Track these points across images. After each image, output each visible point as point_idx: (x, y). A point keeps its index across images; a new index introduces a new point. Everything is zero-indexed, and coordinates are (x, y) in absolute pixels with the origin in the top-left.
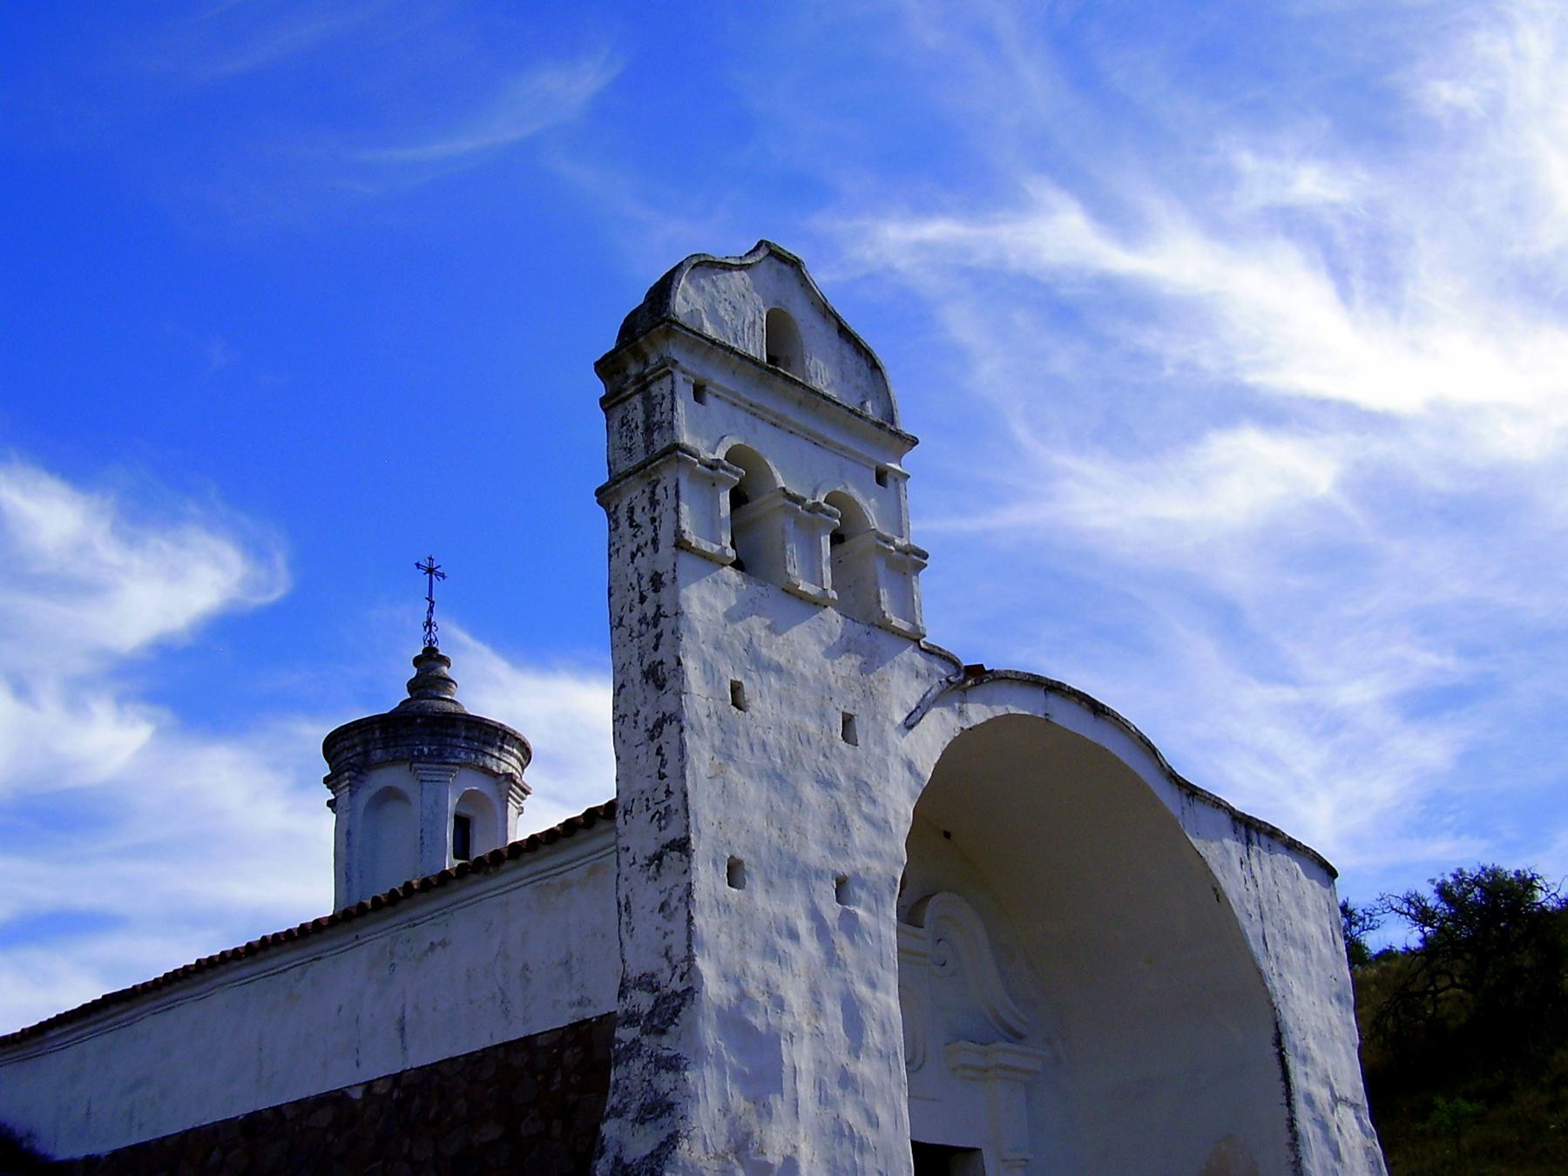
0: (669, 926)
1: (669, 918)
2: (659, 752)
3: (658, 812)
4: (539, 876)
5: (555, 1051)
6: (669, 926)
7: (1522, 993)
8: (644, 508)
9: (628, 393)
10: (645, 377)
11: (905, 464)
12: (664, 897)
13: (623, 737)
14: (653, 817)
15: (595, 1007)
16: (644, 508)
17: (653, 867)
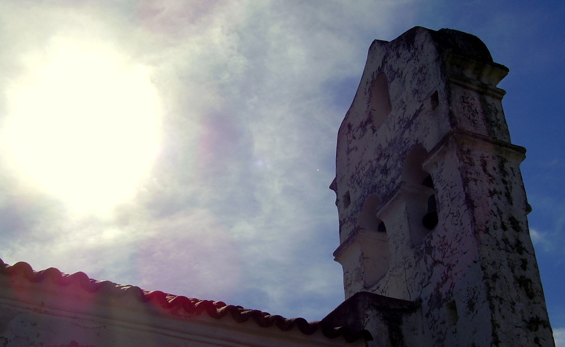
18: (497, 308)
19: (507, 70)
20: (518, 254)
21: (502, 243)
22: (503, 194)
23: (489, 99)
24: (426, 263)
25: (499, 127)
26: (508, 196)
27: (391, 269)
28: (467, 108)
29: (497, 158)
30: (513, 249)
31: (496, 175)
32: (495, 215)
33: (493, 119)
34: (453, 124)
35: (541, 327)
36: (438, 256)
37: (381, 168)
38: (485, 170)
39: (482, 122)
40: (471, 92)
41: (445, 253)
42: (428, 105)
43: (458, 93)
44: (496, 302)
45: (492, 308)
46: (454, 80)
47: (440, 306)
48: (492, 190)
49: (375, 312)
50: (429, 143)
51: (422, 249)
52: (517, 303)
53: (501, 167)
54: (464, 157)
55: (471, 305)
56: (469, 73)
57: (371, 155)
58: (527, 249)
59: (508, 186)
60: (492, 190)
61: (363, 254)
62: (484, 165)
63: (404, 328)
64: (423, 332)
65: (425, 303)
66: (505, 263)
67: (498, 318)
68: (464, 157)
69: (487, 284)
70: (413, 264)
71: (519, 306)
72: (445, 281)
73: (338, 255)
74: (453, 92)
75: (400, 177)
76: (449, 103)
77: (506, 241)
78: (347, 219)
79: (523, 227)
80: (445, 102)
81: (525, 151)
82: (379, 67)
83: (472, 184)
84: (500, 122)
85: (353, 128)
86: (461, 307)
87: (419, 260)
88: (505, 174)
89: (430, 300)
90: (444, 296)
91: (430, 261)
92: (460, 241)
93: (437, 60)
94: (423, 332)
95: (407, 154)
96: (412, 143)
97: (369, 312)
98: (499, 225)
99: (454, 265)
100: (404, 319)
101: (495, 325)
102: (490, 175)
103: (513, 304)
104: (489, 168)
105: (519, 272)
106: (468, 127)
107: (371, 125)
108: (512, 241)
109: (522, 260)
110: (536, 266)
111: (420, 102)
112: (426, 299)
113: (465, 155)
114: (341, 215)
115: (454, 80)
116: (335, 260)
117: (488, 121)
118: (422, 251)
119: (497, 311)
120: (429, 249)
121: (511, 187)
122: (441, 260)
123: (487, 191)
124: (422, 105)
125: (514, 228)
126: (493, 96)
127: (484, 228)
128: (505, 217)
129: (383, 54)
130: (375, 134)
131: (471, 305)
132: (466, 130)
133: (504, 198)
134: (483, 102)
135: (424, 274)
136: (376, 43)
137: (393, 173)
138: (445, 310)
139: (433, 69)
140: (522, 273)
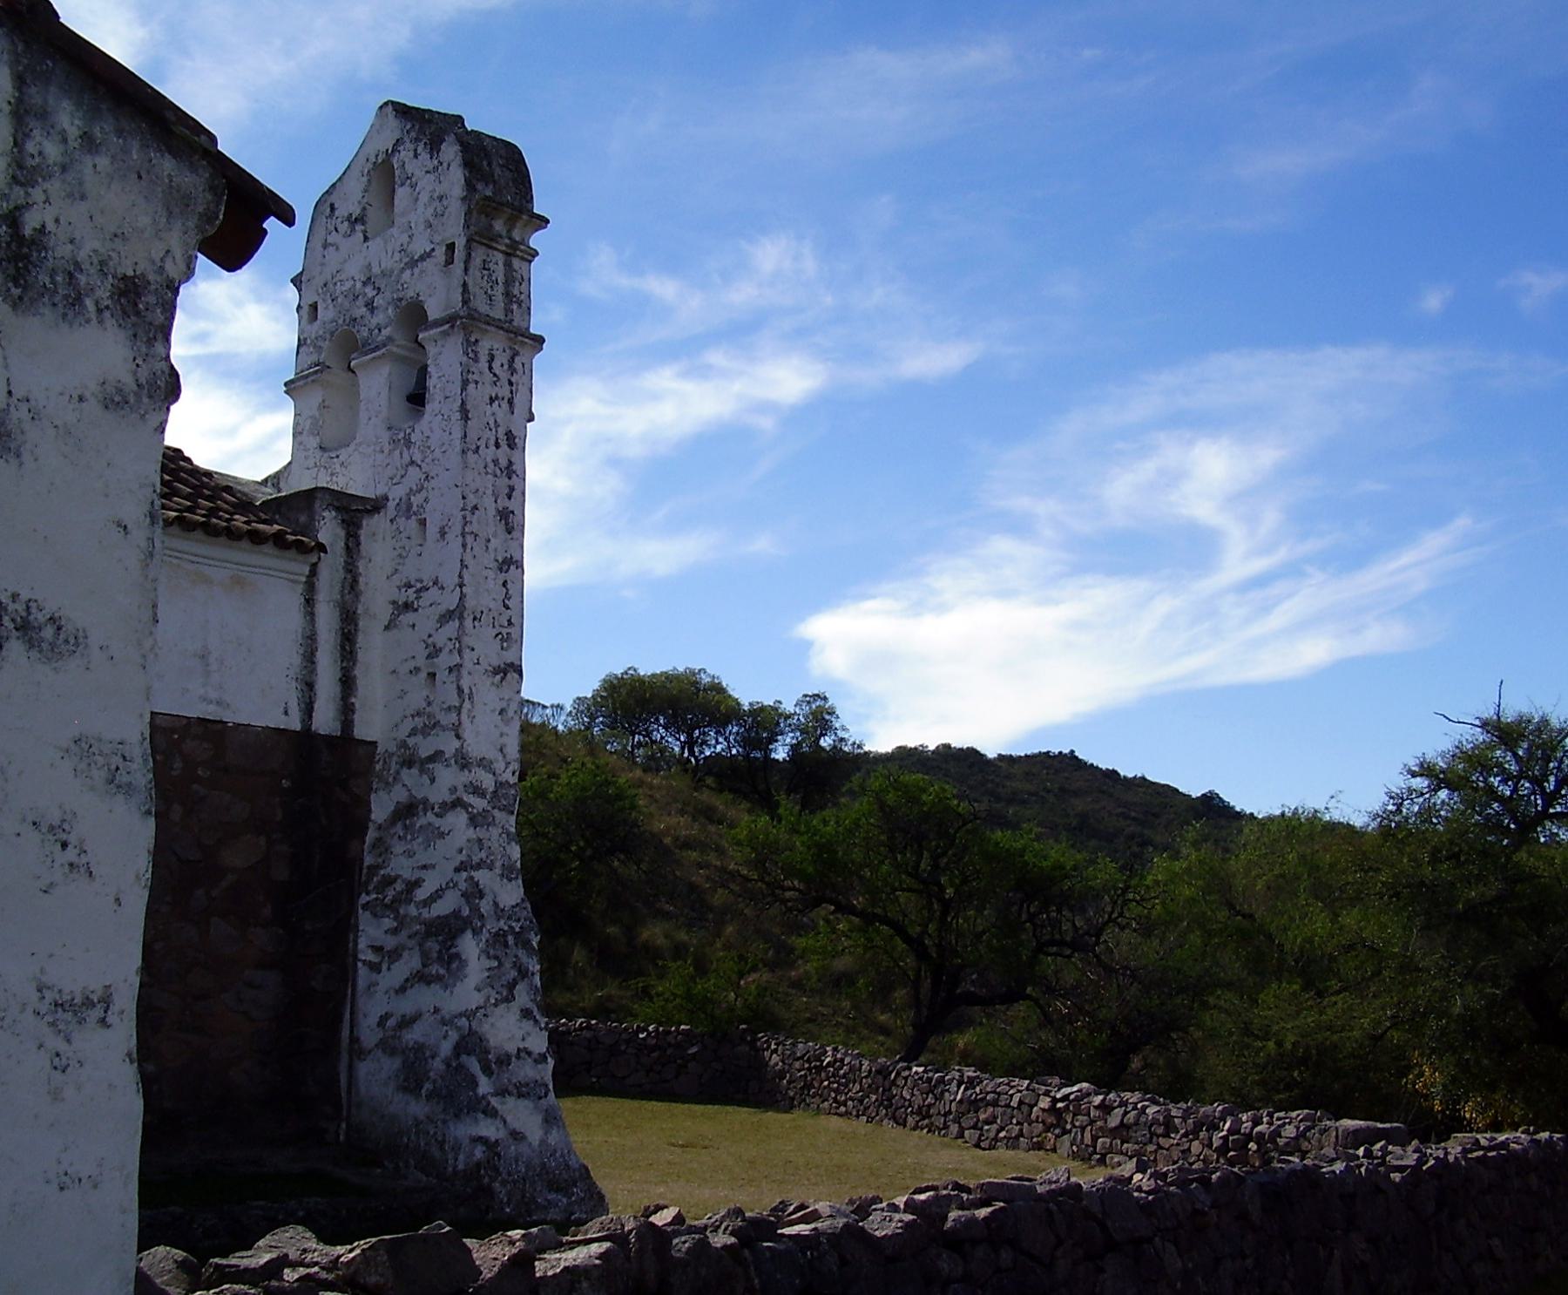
0: (506, 730)
1: (507, 722)
2: (505, 584)
3: (500, 633)
4: (262, 571)
5: (176, 736)
6: (506, 730)
7: (1024, 957)
8: (502, 365)
9: (499, 247)
10: (516, 249)
11: (536, 240)
12: (504, 704)
13: (475, 552)
14: (497, 635)
15: (234, 712)
16: (502, 365)
17: (498, 677)
18: (469, 546)
19: (547, 221)
20: (507, 480)
21: (491, 465)
22: (506, 400)
23: (516, 263)
24: (402, 457)
25: (520, 304)
26: (511, 402)
27: (357, 441)
28: (486, 278)
29: (508, 351)
30: (502, 472)
31: (504, 375)
32: (491, 430)
33: (516, 292)
34: (465, 302)
35: (513, 567)
36: (417, 457)
37: (366, 299)
38: (490, 368)
39: (500, 298)
40: (495, 253)
41: (425, 457)
42: (440, 253)
43: (479, 255)
44: (469, 539)
45: (464, 546)
46: (477, 238)
47: (408, 518)
48: (494, 395)
49: (334, 513)
50: (434, 311)
51: (400, 437)
52: (493, 540)
53: (512, 361)
54: (470, 350)
55: (443, 534)
56: (499, 226)
57: (354, 269)
58: (518, 473)
59: (514, 388)
60: (494, 395)
61: (323, 401)
62: (492, 358)
63: (363, 533)
64: (384, 539)
65: (391, 505)
66: (489, 492)
67: (468, 560)
68: (470, 350)
69: (464, 518)
70: (386, 451)
71: (494, 543)
72: (419, 491)
73: (291, 388)
74: (473, 254)
75: (389, 329)
76: (466, 270)
77: (496, 462)
78: (309, 341)
79: (520, 445)
80: (462, 265)
81: (544, 341)
82: (387, 150)
83: (471, 386)
84: (523, 297)
85: (337, 213)
86: (432, 530)
87: (394, 450)
88: (513, 371)
89: (398, 504)
90: (415, 508)
91: (407, 458)
92: (444, 452)
93: (463, 199)
94: (384, 539)
95: (404, 303)
96: (411, 293)
97: (326, 514)
98: (492, 442)
99: (432, 478)
100: (364, 523)
101: (463, 566)
102: (495, 375)
103: (489, 541)
104: (496, 365)
105: (503, 502)
106: (481, 305)
107: (363, 227)
108: (503, 463)
109: (509, 486)
110: (523, 494)
111: (432, 242)
112: (394, 500)
113: (470, 346)
114: (301, 331)
115: (477, 238)
116: (286, 392)
117: (508, 294)
118: (399, 440)
119: (468, 550)
120: (408, 443)
121: (517, 390)
122: (419, 463)
123: (488, 397)
124: (433, 250)
125: (509, 446)
126: (523, 259)
127: (474, 447)
128: (501, 431)
129: (397, 135)
130: (365, 245)
131: (443, 534)
132: (388, 917)
133: (505, 405)
134: (508, 265)
135: (397, 469)
136: (390, 106)
137: (380, 318)
138: (413, 523)
139: (456, 210)
140: (507, 503)
